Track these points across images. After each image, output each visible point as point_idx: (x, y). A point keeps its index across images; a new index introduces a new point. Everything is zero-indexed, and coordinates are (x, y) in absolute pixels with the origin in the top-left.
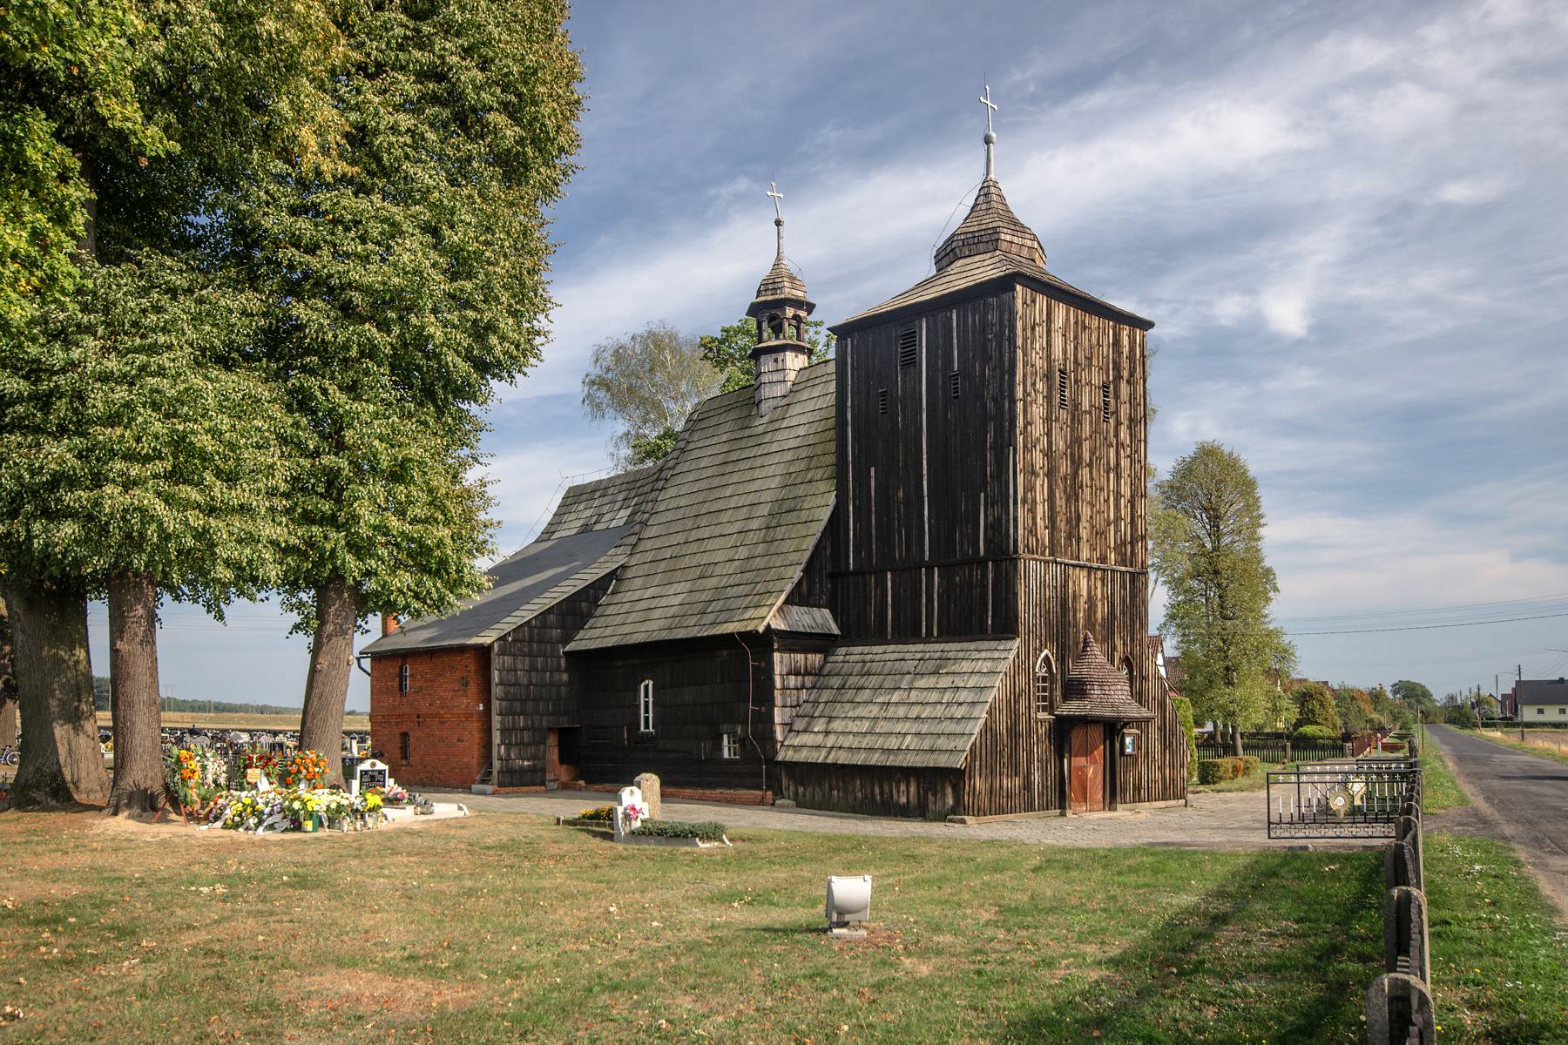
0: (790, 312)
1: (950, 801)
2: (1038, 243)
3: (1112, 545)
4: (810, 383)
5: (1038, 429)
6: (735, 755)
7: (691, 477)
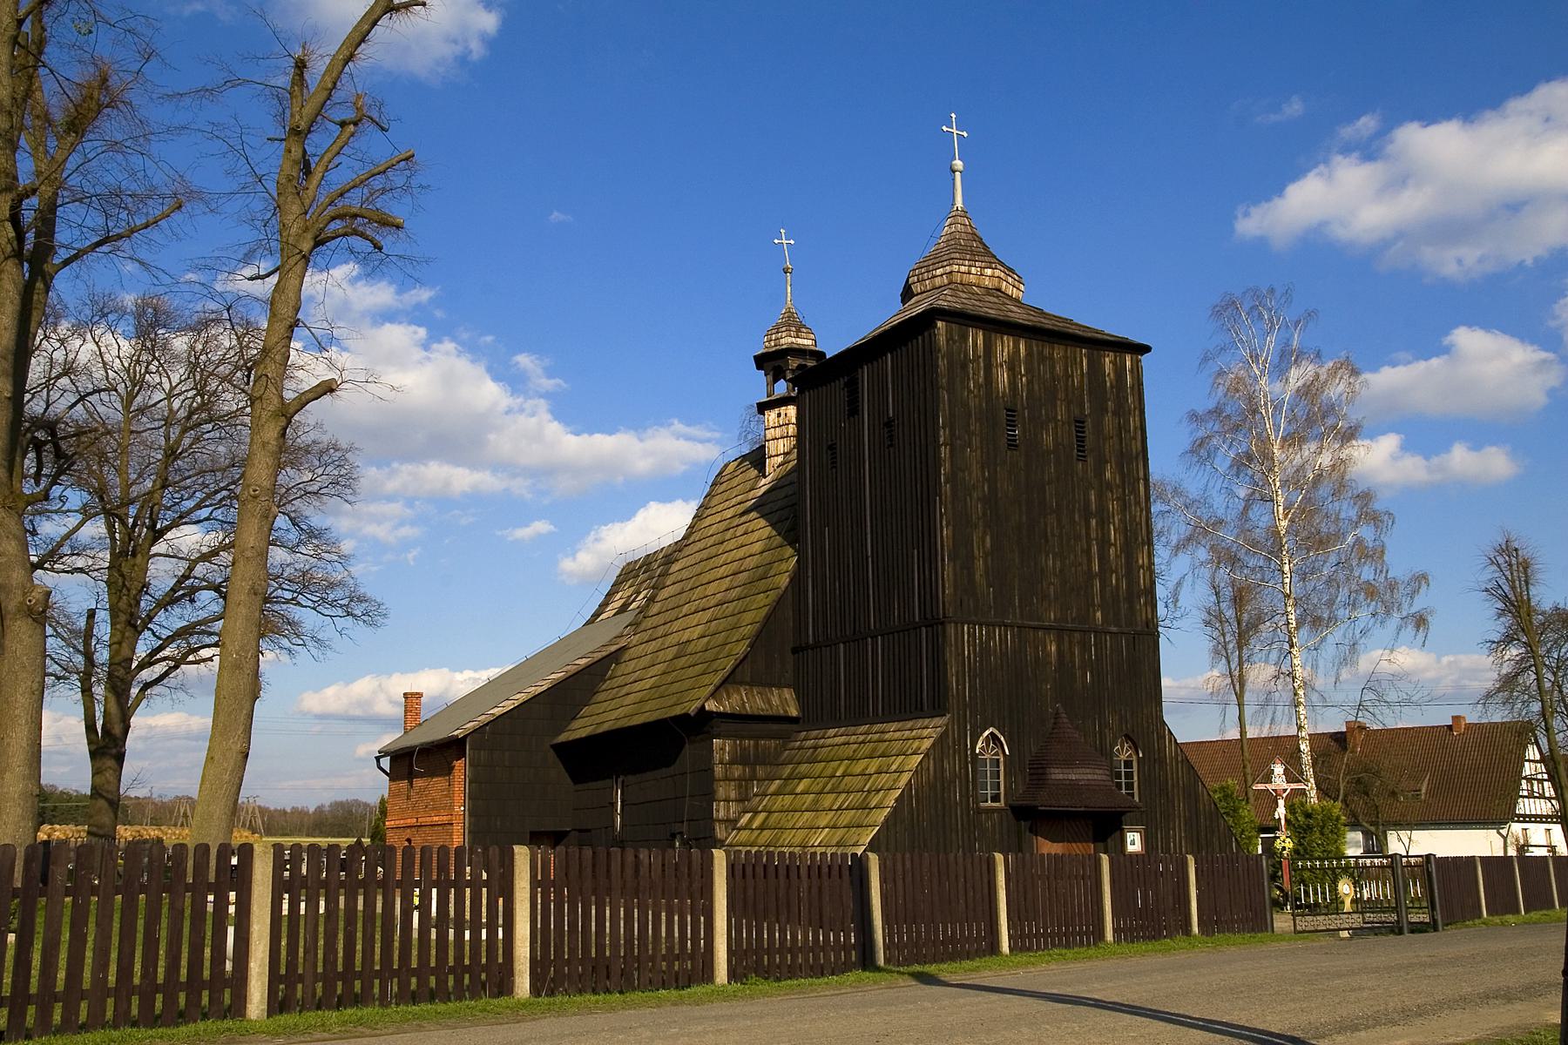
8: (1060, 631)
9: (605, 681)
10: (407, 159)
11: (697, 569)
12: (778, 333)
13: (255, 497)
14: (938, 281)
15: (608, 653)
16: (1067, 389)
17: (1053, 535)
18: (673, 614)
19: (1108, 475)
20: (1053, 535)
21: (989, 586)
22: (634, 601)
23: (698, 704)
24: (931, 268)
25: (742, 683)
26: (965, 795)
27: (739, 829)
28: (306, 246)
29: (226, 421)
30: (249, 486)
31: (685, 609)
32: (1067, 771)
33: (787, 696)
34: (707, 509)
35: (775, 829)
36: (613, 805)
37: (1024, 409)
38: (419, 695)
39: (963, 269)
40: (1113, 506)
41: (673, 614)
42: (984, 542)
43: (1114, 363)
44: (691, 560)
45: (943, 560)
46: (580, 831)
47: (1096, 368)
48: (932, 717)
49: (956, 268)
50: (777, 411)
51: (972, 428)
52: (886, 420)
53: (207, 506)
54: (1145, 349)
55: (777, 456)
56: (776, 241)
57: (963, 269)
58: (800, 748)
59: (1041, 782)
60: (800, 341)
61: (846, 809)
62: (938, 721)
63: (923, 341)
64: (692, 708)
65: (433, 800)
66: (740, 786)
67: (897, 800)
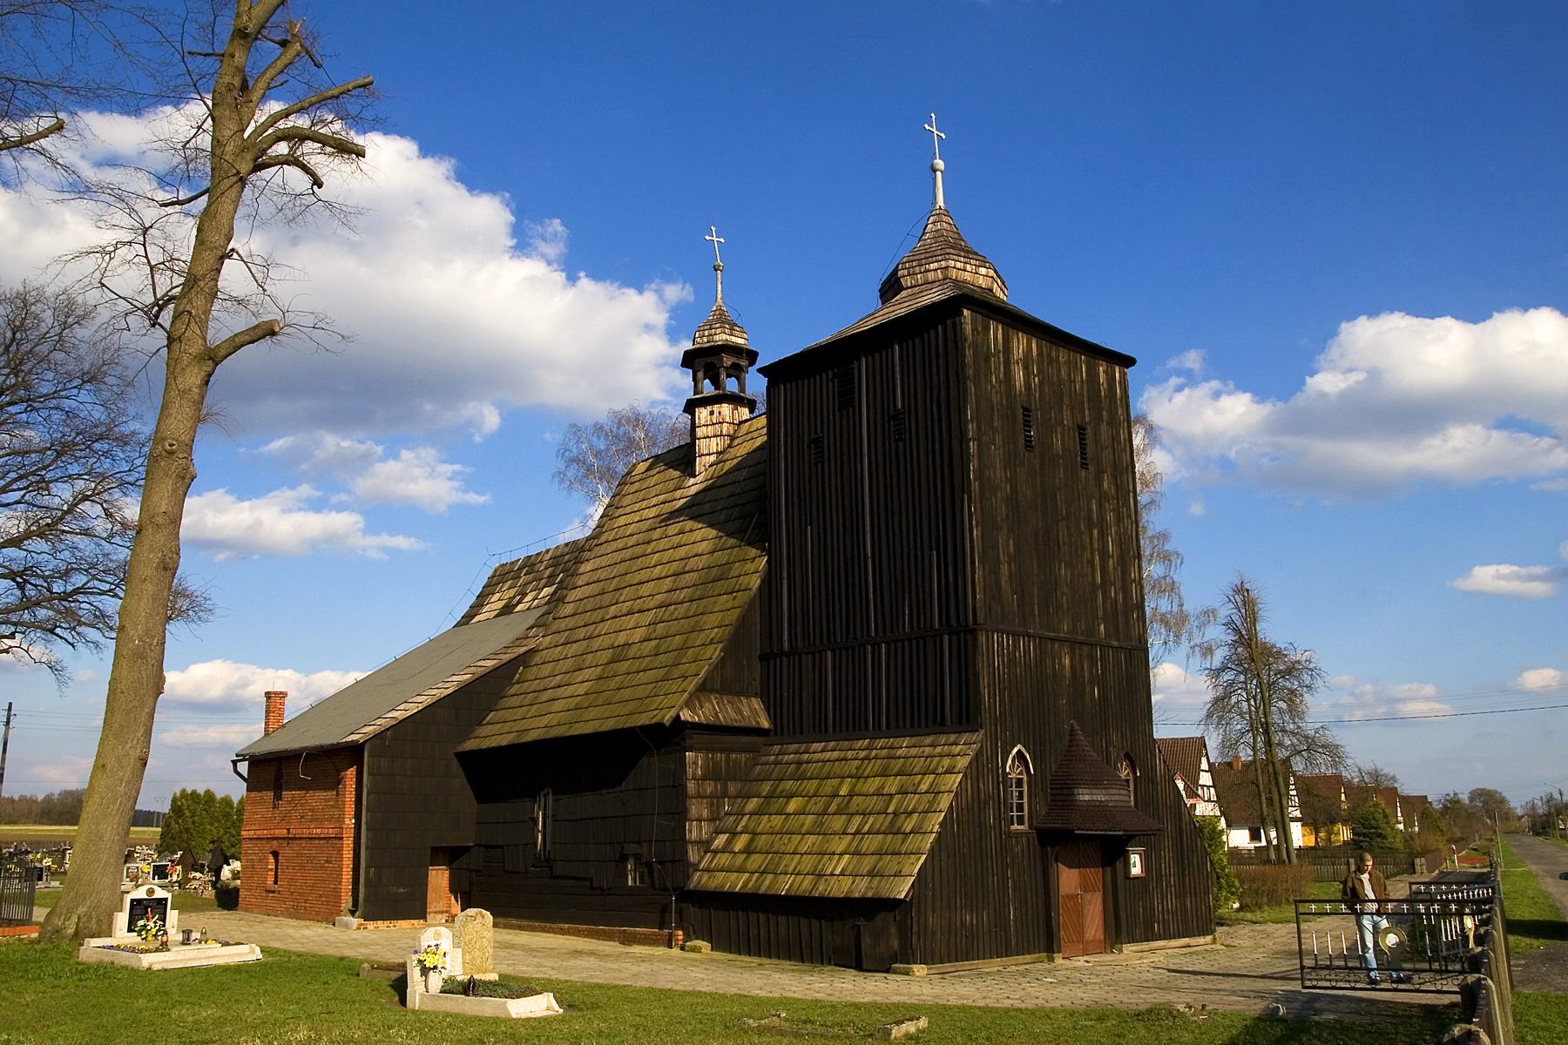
0: (728, 361)
1: (895, 943)
2: (995, 272)
3: (1100, 613)
4: (750, 436)
5: (998, 474)
6: (642, 882)
7: (615, 545)
8: (1073, 644)
9: (513, 685)
10: (364, 86)
11: (621, 569)
12: (711, 329)
13: (172, 453)
14: (931, 276)
15: (516, 655)
16: (1070, 395)
17: (1064, 544)
18: (597, 615)
19: (1105, 485)
20: (1064, 544)
21: (1014, 593)
22: (519, 602)
23: (673, 713)
24: (924, 261)
25: (712, 691)
26: (998, 818)
27: (715, 852)
28: (244, 167)
29: (42, 402)
30: (164, 439)
31: (613, 610)
32: (1094, 791)
33: (757, 707)
34: (617, 508)
35: (768, 853)
36: (535, 821)
37: (1037, 410)
38: (283, 695)
39: (959, 265)
40: (1110, 517)
41: (597, 615)
42: (1008, 545)
43: (1105, 372)
44: (604, 561)
45: (973, 562)
46: (487, 847)
47: (1092, 374)
48: (960, 732)
49: (952, 263)
50: (709, 408)
51: (996, 424)
52: (892, 413)
53: (15, 490)
54: (1128, 362)
55: (709, 454)
56: (707, 238)
57: (959, 265)
58: (776, 763)
59: (1067, 803)
60: (734, 339)
61: (868, 833)
62: (974, 737)
63: (945, 331)
64: (667, 718)
65: (312, 810)
66: (712, 805)
67: (941, 825)
